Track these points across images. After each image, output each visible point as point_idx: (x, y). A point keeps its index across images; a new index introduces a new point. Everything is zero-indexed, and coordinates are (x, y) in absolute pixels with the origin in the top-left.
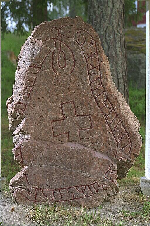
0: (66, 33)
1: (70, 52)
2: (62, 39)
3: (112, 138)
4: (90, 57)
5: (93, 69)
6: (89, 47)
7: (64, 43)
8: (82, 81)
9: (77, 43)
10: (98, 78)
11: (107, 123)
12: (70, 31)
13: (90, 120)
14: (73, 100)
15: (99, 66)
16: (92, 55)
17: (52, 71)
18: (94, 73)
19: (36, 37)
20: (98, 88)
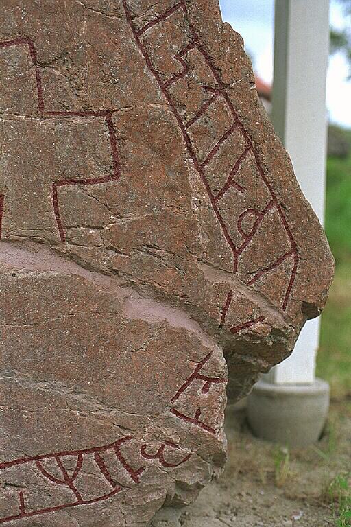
3: (210, 231)
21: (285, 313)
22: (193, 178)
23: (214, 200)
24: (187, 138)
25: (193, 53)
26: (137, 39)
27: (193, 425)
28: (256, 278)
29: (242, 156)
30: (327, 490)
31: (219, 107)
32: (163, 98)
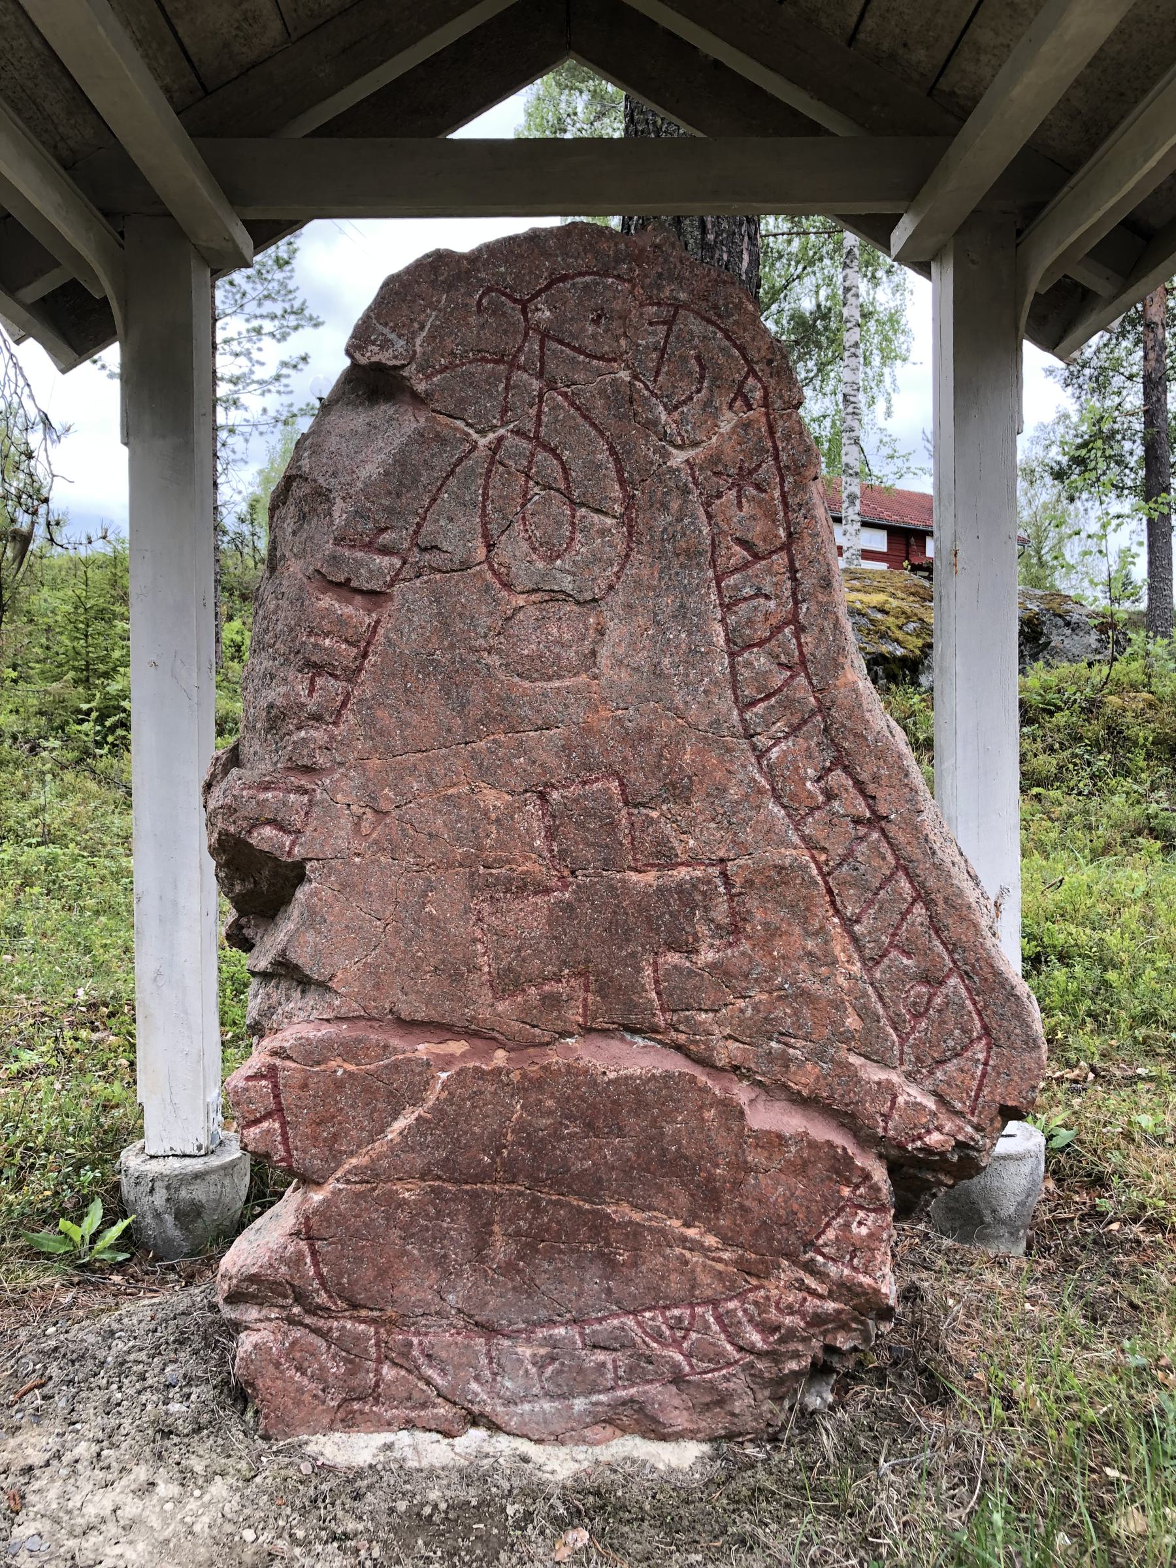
0: (574, 328)
1: (603, 456)
2: (551, 366)
5: (746, 565)
6: (727, 422)
7: (565, 395)
10: (779, 629)
11: (837, 912)
13: (728, 893)
15: (786, 547)
18: (756, 596)
19: (376, 349)
20: (780, 689)
22: (840, 947)
24: (830, 891)
25: (838, 777)
31: (874, 848)
32: (795, 839)
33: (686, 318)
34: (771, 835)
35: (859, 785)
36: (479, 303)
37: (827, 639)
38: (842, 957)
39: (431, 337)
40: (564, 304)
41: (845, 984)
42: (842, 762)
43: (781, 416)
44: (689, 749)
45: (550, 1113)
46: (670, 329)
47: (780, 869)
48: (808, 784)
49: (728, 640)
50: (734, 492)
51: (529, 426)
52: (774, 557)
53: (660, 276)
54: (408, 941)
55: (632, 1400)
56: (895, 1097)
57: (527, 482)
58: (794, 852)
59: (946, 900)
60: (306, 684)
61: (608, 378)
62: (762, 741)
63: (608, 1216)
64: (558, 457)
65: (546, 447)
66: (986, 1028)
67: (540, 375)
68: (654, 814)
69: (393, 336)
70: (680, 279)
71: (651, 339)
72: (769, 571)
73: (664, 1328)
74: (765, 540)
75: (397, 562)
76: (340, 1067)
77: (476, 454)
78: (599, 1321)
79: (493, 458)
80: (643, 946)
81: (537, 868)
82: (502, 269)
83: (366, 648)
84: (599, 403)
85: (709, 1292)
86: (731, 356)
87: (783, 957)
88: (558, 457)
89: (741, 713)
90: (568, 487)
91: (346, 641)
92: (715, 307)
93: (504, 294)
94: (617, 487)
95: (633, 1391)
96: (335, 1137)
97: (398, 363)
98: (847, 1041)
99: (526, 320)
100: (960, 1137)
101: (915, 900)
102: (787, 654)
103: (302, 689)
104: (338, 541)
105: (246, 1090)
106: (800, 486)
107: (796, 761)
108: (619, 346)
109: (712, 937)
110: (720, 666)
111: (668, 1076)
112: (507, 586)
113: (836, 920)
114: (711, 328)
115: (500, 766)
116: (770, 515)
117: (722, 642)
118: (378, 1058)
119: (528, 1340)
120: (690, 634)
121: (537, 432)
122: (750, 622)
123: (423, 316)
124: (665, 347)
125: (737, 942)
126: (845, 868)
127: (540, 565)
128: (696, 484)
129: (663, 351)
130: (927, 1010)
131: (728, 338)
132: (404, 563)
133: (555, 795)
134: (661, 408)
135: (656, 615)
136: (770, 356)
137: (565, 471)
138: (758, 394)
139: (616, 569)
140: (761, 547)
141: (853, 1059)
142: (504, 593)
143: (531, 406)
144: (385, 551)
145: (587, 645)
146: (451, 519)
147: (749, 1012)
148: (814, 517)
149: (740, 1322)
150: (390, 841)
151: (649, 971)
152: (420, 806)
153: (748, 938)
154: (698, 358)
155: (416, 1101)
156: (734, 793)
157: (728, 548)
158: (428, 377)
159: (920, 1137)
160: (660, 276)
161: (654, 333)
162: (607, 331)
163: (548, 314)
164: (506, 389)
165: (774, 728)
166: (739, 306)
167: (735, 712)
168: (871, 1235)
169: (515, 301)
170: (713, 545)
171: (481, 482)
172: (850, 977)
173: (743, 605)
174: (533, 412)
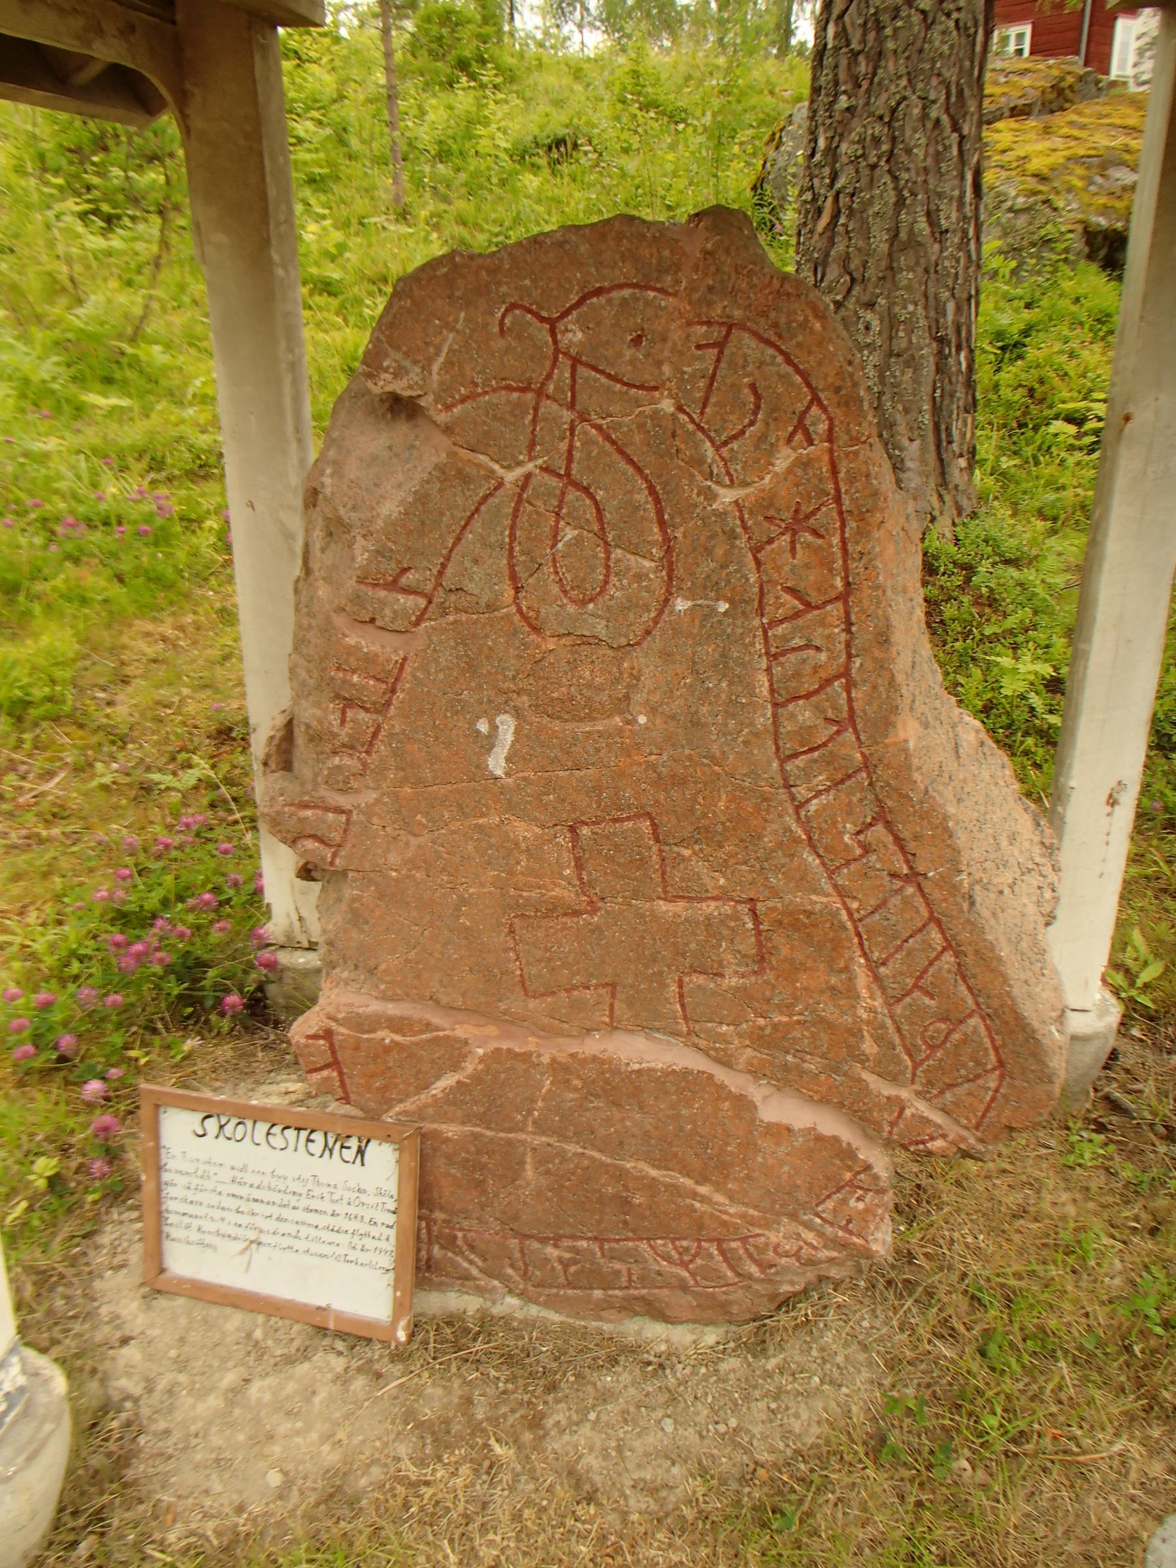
0: (610, 353)
1: (642, 497)
2: (582, 398)
3: (878, 1039)
4: (787, 538)
5: (797, 615)
6: (783, 460)
7: (599, 428)
8: (717, 696)
9: (691, 427)
10: (828, 682)
11: (865, 955)
12: (640, 337)
13: (756, 928)
14: (649, 809)
15: (843, 597)
16: (799, 521)
17: (507, 617)
18: (807, 646)
19: (388, 377)
20: (824, 745)
21: (979, 1134)
22: (862, 979)
23: (889, 1005)
24: (859, 935)
25: (879, 831)
26: (797, 813)
27: (840, 1233)
28: (942, 1092)
29: (937, 958)
30: (496, 599)
31: (907, 902)
32: (828, 888)
33: (740, 340)
34: (803, 880)
35: (898, 841)
36: (502, 323)
37: (879, 697)
38: (864, 993)
39: (448, 364)
40: (598, 324)
41: (865, 1016)
42: (881, 816)
43: (847, 454)
44: (724, 797)
45: (576, 1089)
46: (721, 352)
47: (809, 914)
48: (846, 838)
49: (772, 691)
50: (787, 538)
51: (560, 465)
52: (829, 608)
53: (711, 289)
54: (445, 945)
55: (642, 1298)
56: (902, 1110)
57: (557, 522)
58: (825, 900)
59: (977, 952)
60: (338, 714)
61: (647, 409)
62: (802, 792)
63: (628, 1171)
64: (592, 497)
65: (577, 486)
66: (1001, 1063)
67: (572, 406)
68: (687, 853)
69: (407, 363)
70: (734, 293)
71: (698, 365)
72: (822, 623)
73: (673, 1253)
74: (819, 590)
75: (422, 602)
76: (387, 1036)
77: (501, 492)
78: (618, 1241)
79: (520, 495)
80: (669, 967)
81: (566, 893)
82: (527, 282)
83: (394, 684)
84: (637, 438)
85: (715, 1234)
86: (792, 384)
87: (806, 989)
88: (592, 497)
89: (781, 765)
90: (602, 529)
91: (374, 678)
92: (775, 325)
93: (530, 311)
94: (656, 530)
95: (644, 1291)
96: (386, 1088)
97: (414, 394)
98: (862, 1062)
99: (555, 342)
100: (962, 1146)
101: (944, 949)
102: (834, 708)
103: (334, 719)
104: (361, 581)
105: (307, 1046)
106: (863, 533)
107: (835, 815)
108: (661, 373)
109: (739, 965)
110: (763, 719)
111: (686, 1072)
112: (536, 629)
113: (862, 961)
114: (771, 351)
115: (529, 802)
116: (826, 563)
117: (765, 692)
118: (422, 1032)
119: (556, 1246)
120: (731, 684)
121: (568, 468)
122: (797, 675)
123: (437, 340)
124: (714, 374)
125: (762, 970)
126: (877, 917)
127: (571, 609)
128: (745, 527)
129: (713, 378)
130: (944, 1042)
131: (789, 361)
132: (430, 602)
133: (585, 831)
134: (708, 444)
135: (694, 663)
136: (838, 383)
137: (599, 511)
138: (823, 427)
139: (653, 615)
140: (814, 599)
141: (865, 1075)
142: (533, 637)
143: (562, 439)
144: (408, 591)
145: (621, 689)
146: (476, 562)
147: (768, 1031)
148: (875, 568)
149: (740, 1259)
150: (425, 861)
151: (674, 988)
152: (453, 832)
153: (772, 969)
154: (753, 387)
155: (455, 1067)
156: (768, 841)
157: (778, 598)
158: (448, 408)
159: (923, 1142)
160: (711, 289)
161: (700, 358)
162: (647, 356)
163: (580, 335)
164: (534, 421)
165: (815, 781)
166: (804, 325)
167: (775, 765)
168: (867, 1210)
169: (543, 320)
170: (762, 593)
171: (508, 522)
172: (871, 1010)
173: (792, 657)
174: (563, 446)
